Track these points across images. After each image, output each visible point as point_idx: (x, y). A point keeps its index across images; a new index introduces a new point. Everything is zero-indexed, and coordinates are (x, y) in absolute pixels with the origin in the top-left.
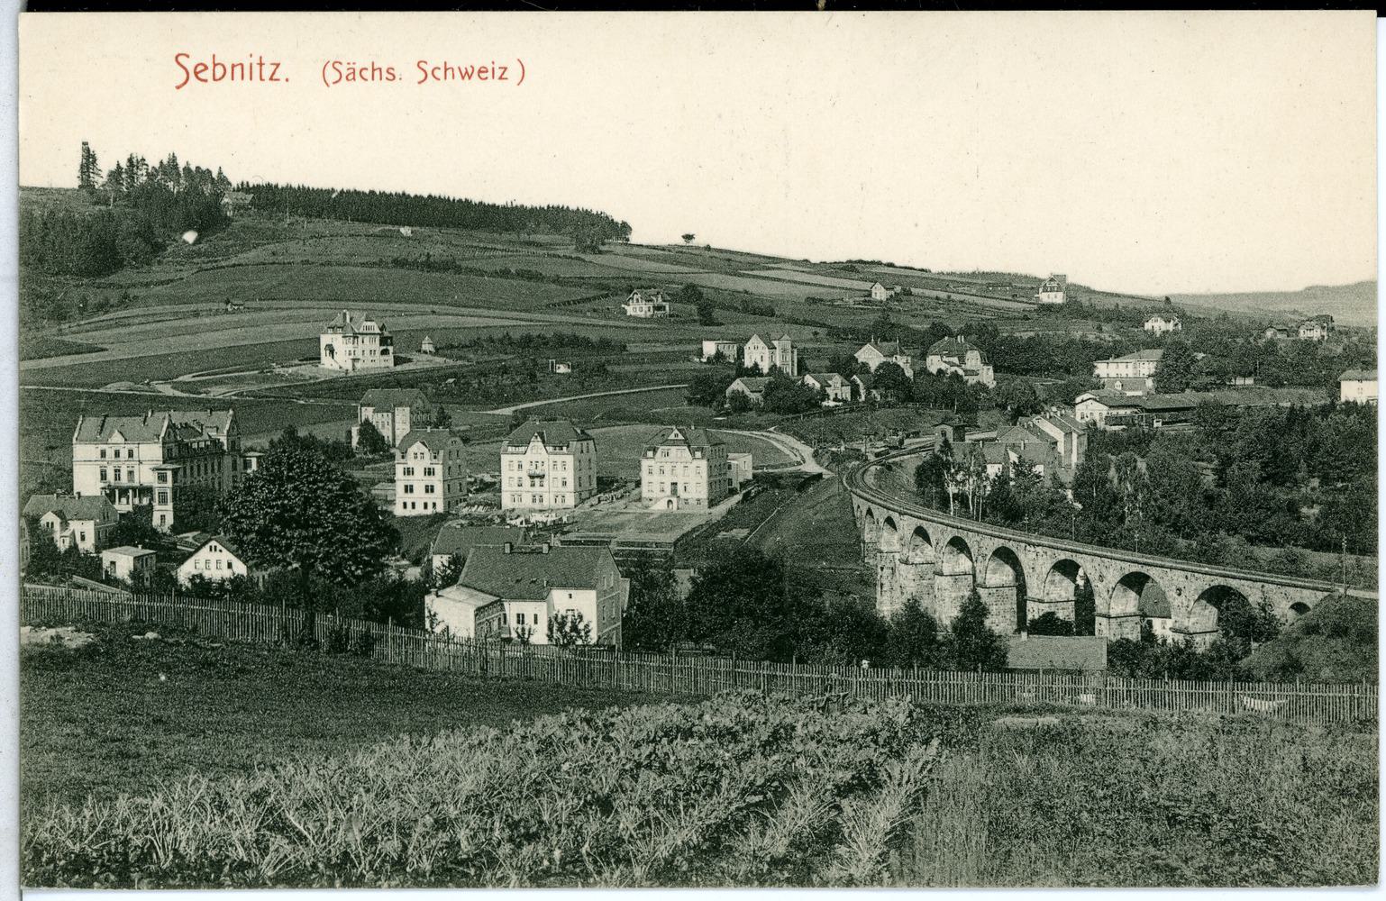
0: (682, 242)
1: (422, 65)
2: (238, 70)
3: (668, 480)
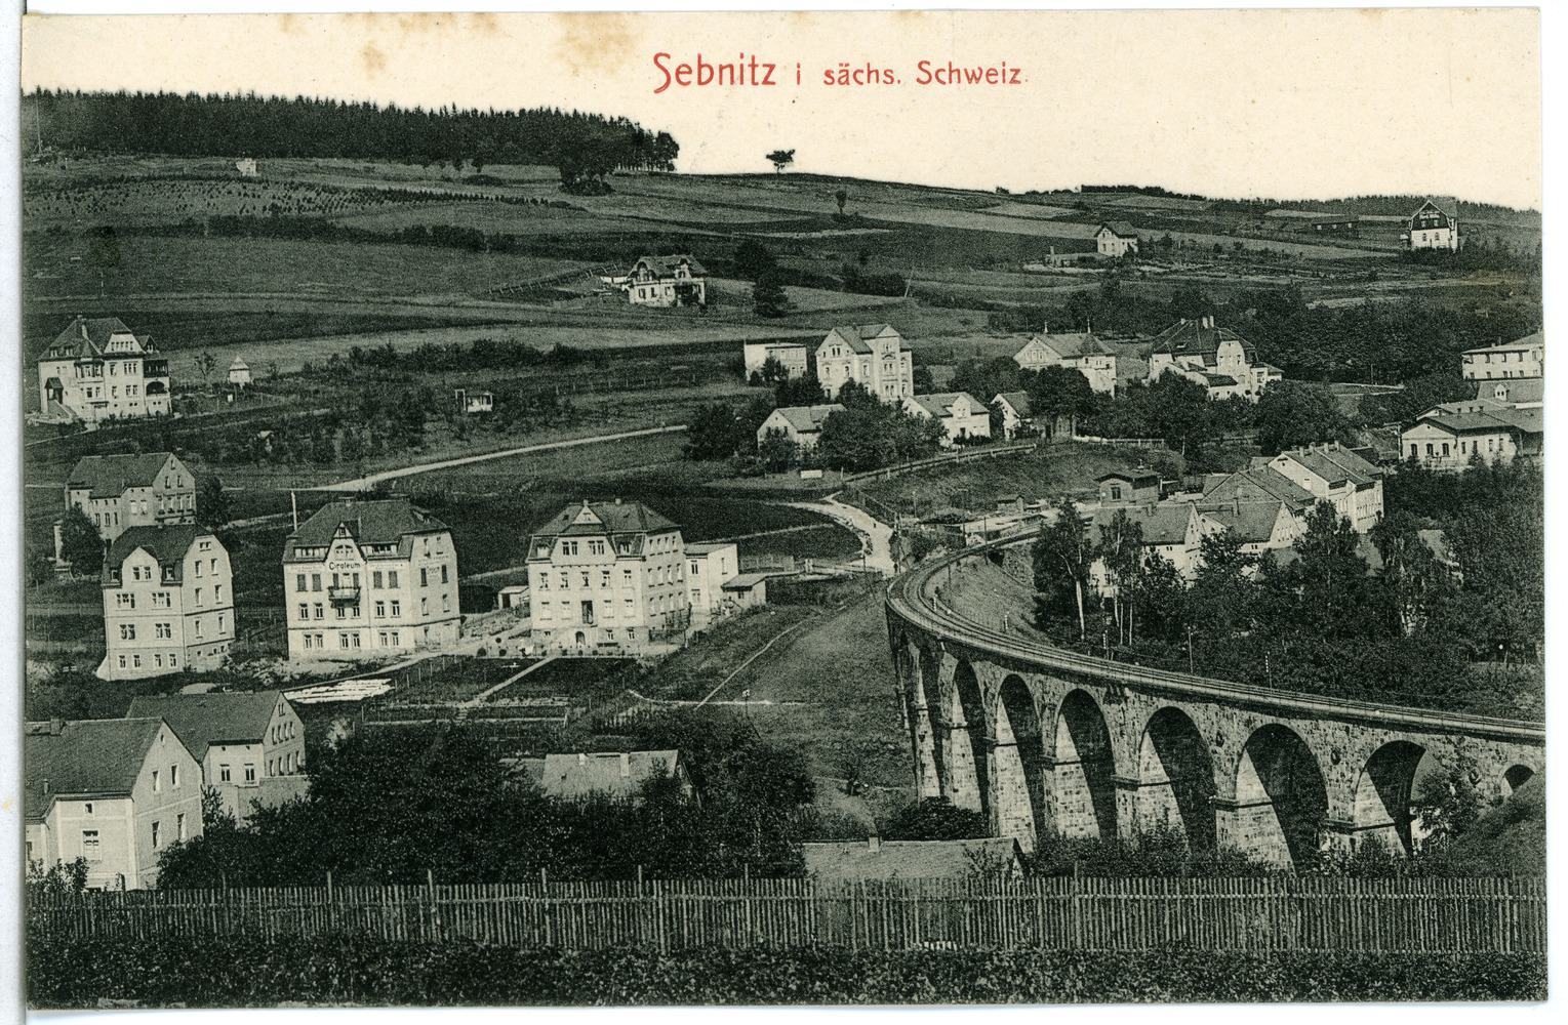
0: (769, 167)
1: (924, 66)
2: (727, 72)
3: (577, 595)
